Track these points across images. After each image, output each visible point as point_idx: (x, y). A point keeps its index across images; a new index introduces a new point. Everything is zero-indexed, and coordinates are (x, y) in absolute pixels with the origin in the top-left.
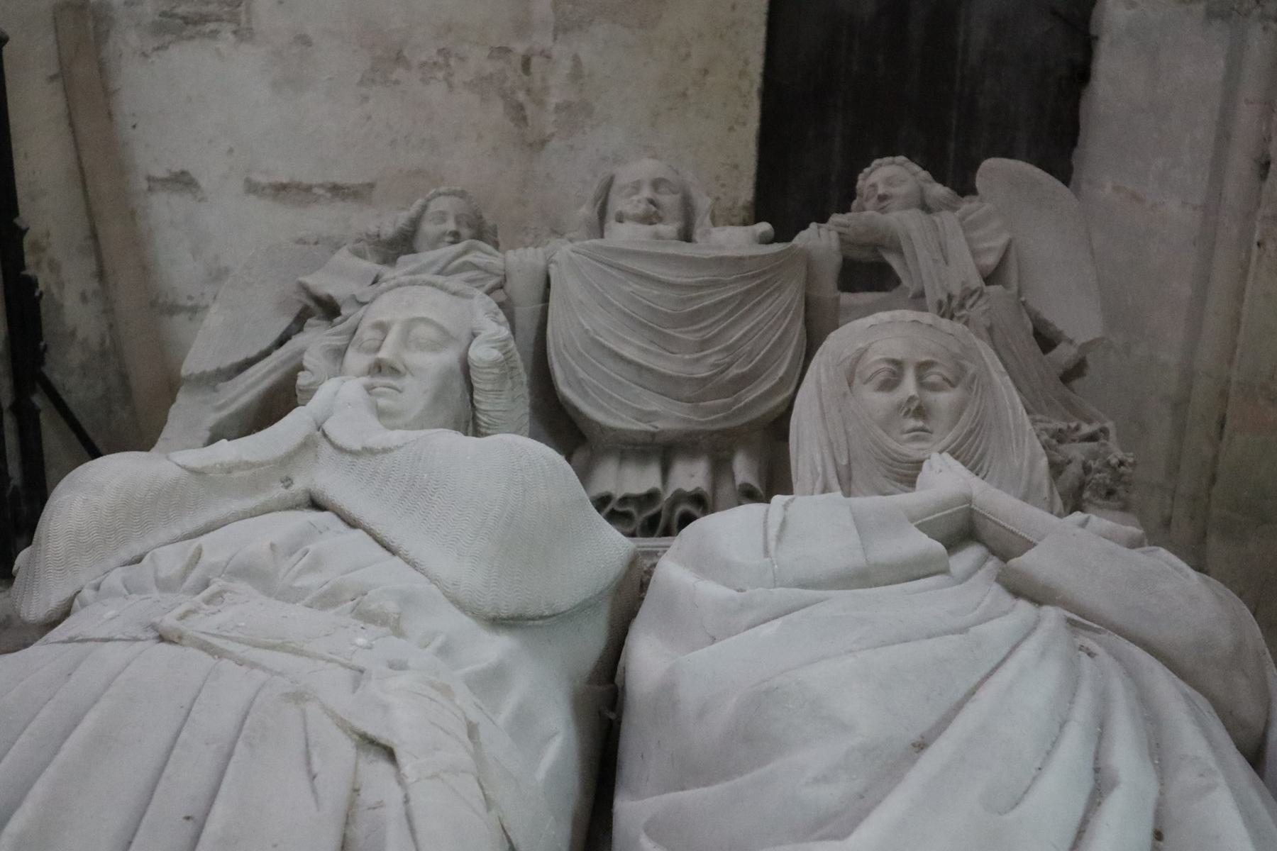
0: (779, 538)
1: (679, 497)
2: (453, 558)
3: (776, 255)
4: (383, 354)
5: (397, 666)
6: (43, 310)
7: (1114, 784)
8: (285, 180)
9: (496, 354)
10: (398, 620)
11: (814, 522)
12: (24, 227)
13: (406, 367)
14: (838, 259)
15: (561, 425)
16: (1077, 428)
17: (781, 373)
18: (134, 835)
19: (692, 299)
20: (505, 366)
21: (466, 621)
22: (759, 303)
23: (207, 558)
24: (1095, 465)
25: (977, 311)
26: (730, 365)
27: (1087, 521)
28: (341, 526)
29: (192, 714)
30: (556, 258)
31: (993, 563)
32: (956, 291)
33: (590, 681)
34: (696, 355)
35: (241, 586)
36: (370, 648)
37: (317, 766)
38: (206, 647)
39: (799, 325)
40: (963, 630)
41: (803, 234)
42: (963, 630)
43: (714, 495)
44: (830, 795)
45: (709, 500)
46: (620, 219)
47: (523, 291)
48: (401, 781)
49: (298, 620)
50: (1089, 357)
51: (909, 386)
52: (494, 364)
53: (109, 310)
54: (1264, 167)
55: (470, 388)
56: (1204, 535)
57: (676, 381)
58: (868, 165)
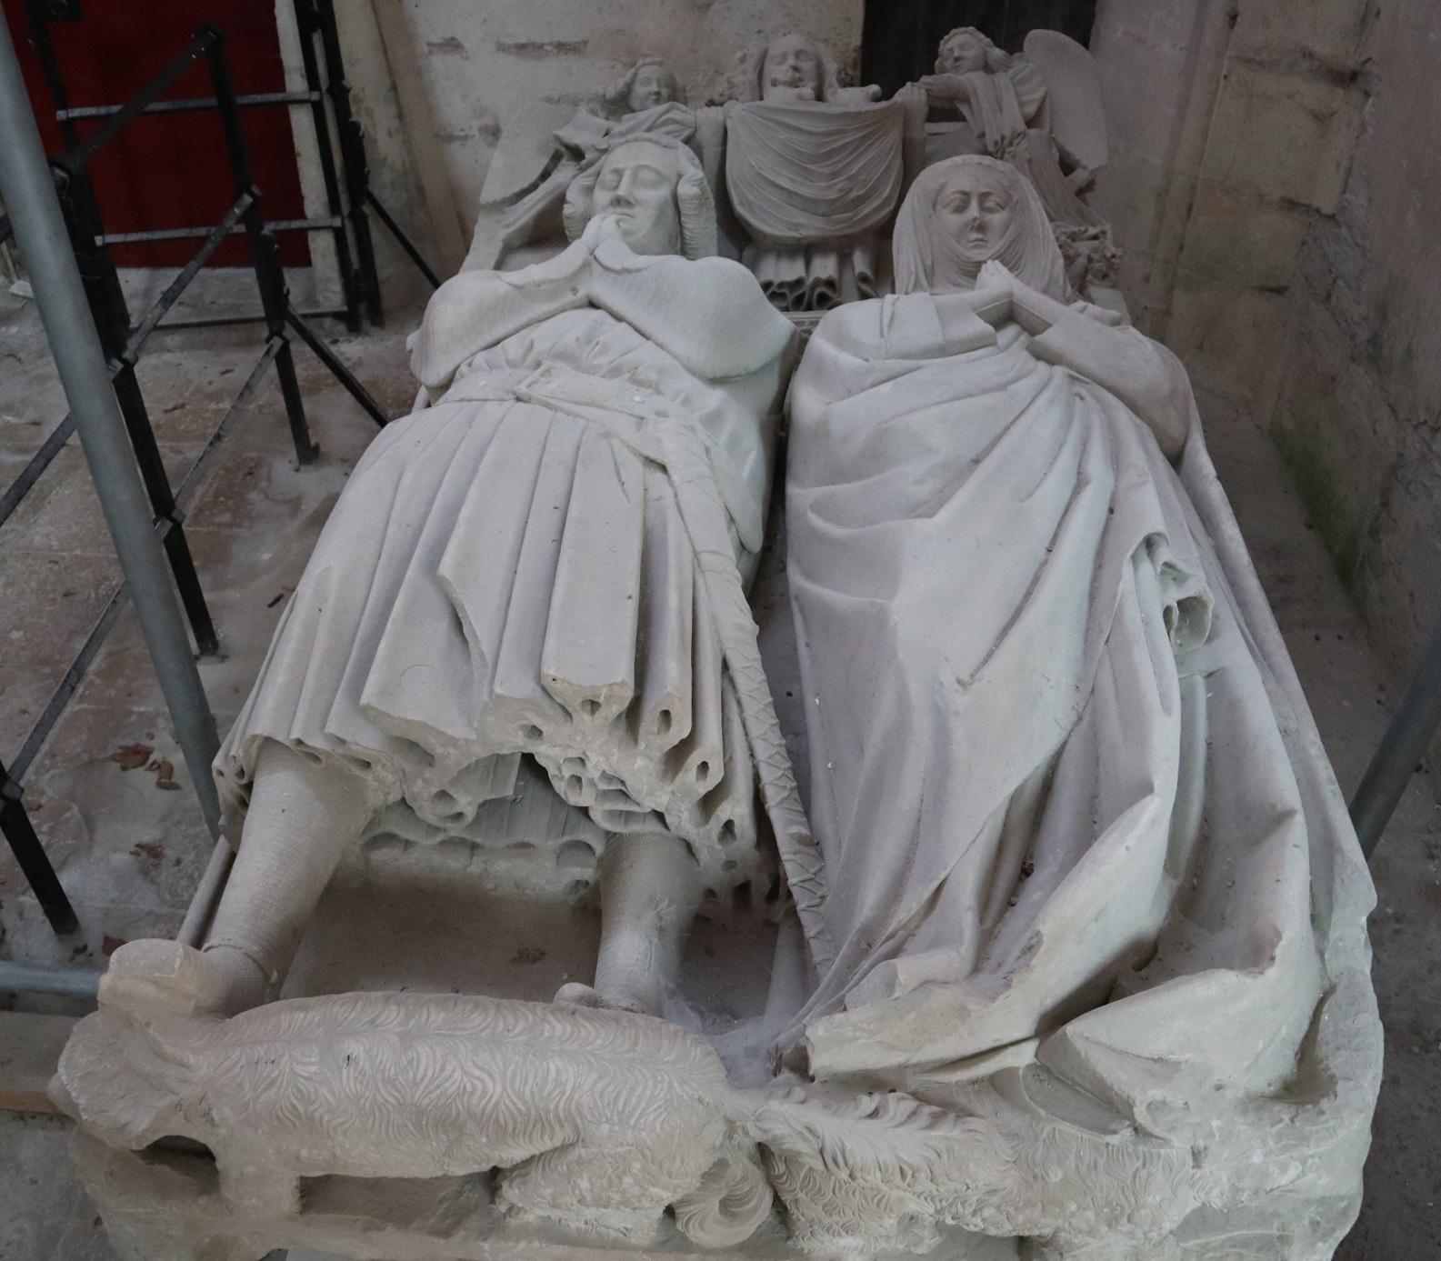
0: (890, 325)
1: (817, 282)
2: (687, 342)
3: (883, 110)
4: (621, 192)
5: (662, 414)
6: (365, 144)
7: (1087, 483)
8: (524, 41)
9: (696, 190)
10: (657, 385)
11: (907, 314)
12: (348, 86)
13: (636, 200)
14: (926, 109)
15: (739, 238)
16: (1086, 231)
17: (886, 193)
18: (528, 518)
19: (826, 143)
20: (702, 197)
21: (697, 382)
22: (871, 144)
23: (537, 347)
24: (1096, 256)
25: (1021, 148)
26: (850, 190)
27: (1085, 308)
28: (611, 320)
29: (547, 447)
30: (732, 114)
31: (1024, 337)
32: (1008, 134)
33: (770, 413)
34: (830, 183)
35: (560, 364)
36: (643, 403)
37: (624, 478)
38: (547, 405)
39: (898, 161)
40: (1002, 387)
41: (901, 91)
42: (1002, 387)
43: (840, 279)
44: (924, 491)
45: (837, 285)
46: (774, 83)
47: (708, 138)
48: (672, 484)
49: (598, 386)
50: (1098, 179)
51: (973, 211)
52: (695, 197)
53: (407, 142)
54: (1233, 18)
55: (679, 213)
56: (1172, 288)
57: (815, 201)
58: (947, 33)
